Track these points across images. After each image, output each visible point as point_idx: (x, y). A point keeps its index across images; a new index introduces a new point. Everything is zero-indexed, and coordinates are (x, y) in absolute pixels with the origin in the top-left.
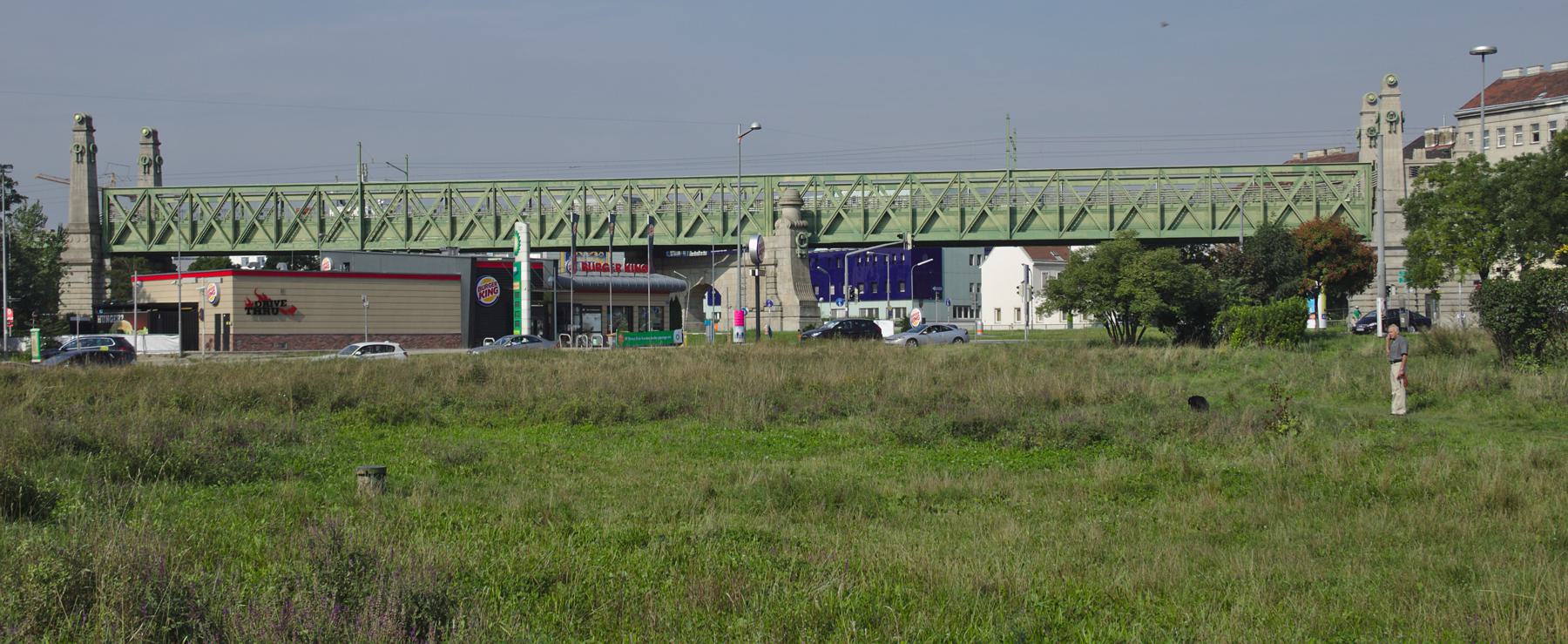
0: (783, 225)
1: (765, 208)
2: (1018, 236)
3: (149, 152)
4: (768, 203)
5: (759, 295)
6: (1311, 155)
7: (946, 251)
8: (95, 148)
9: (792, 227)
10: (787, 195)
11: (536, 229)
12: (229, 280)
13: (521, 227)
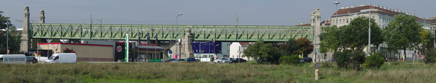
0: (186, 36)
1: (182, 32)
2: (238, 40)
3: (42, 15)
4: (183, 31)
5: (181, 50)
6: (301, 24)
7: (222, 43)
10: (187, 30)
11: (130, 35)
12: (60, 45)
13: (127, 35)
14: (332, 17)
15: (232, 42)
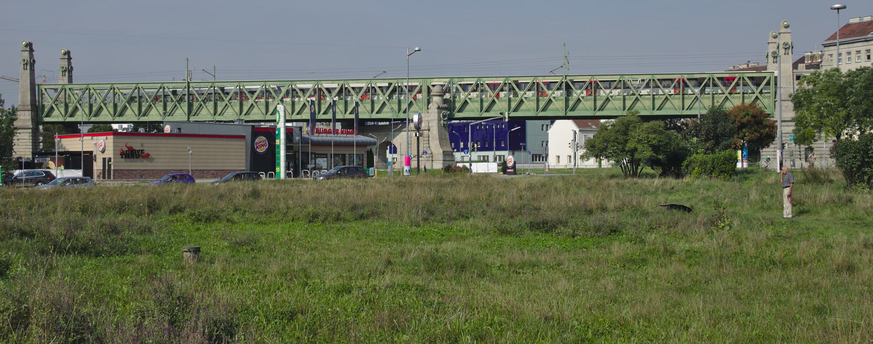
2: (570, 114)
8: (34, 61)
9: (439, 108)
14: (825, 46)
15: (553, 119)
